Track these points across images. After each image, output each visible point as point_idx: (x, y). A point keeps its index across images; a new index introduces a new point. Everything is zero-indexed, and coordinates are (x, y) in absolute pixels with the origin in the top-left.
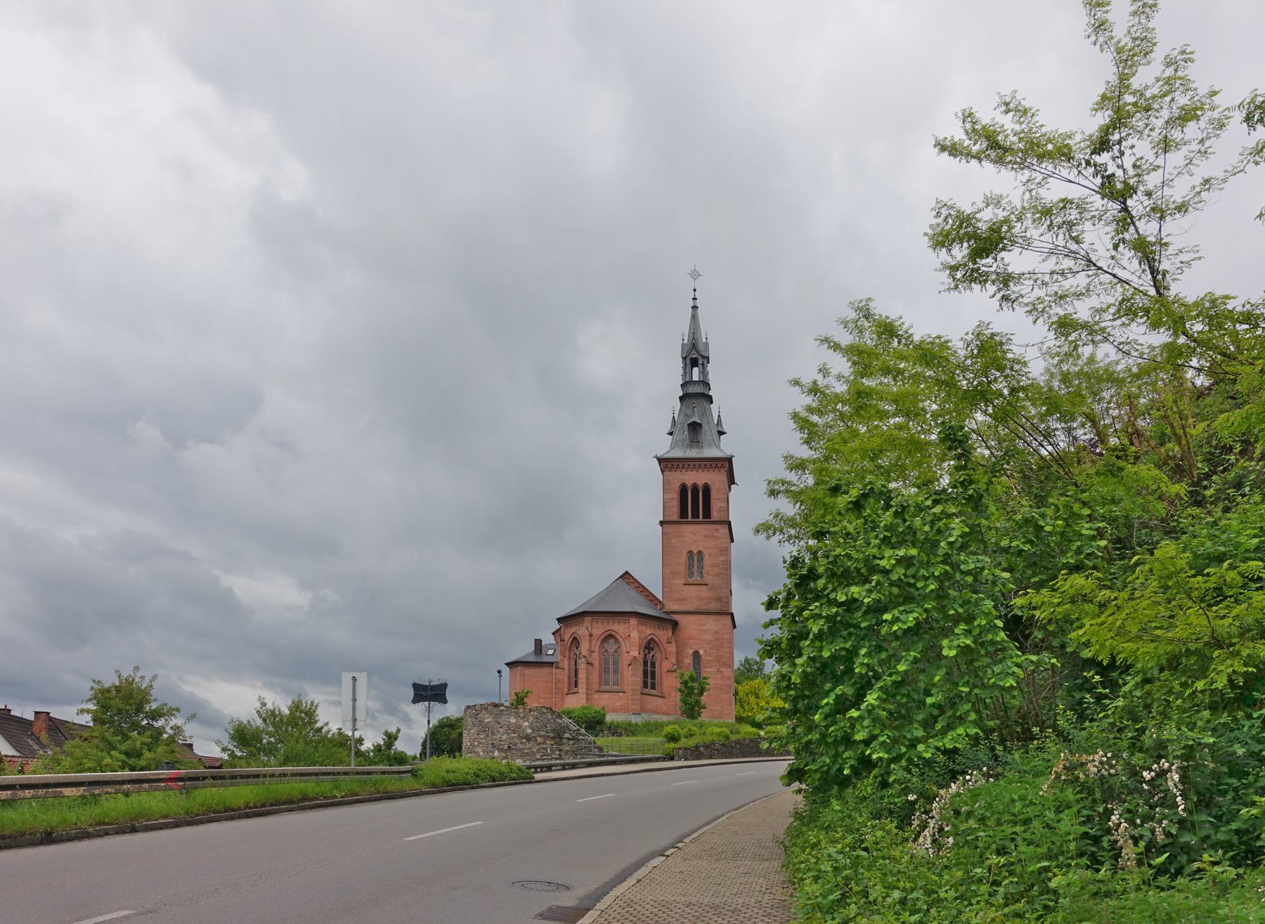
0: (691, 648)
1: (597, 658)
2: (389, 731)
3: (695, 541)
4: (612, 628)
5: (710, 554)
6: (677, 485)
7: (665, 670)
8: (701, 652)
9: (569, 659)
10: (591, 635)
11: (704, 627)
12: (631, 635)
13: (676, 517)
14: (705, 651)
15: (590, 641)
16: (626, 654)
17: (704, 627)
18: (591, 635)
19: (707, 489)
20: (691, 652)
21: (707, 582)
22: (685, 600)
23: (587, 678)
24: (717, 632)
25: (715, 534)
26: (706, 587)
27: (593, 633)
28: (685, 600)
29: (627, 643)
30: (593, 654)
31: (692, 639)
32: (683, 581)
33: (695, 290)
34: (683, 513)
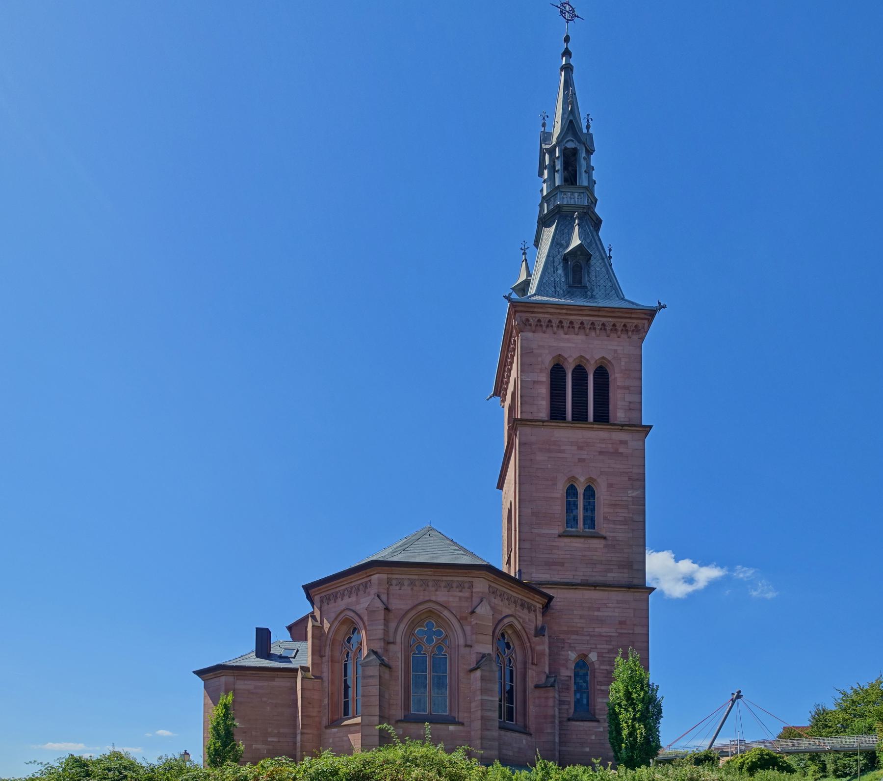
0: (572, 648)
1: (400, 656)
2: (661, 718)
3: (581, 460)
4: (433, 598)
5: (610, 485)
6: (548, 362)
7: (531, 685)
8: (593, 657)
9: (333, 661)
10: (387, 609)
11: (596, 613)
12: (478, 610)
13: (544, 414)
14: (600, 655)
15: (386, 622)
16: (464, 651)
17: (596, 613)
18: (387, 609)
19: (602, 374)
20: (573, 656)
21: (603, 533)
22: (562, 564)
23: (381, 695)
24: (621, 623)
25: (621, 450)
26: (603, 542)
27: (391, 607)
28: (562, 564)
29: (468, 629)
30: (391, 647)
31: (576, 633)
32: (556, 531)
33: (567, 39)
34: (557, 414)
